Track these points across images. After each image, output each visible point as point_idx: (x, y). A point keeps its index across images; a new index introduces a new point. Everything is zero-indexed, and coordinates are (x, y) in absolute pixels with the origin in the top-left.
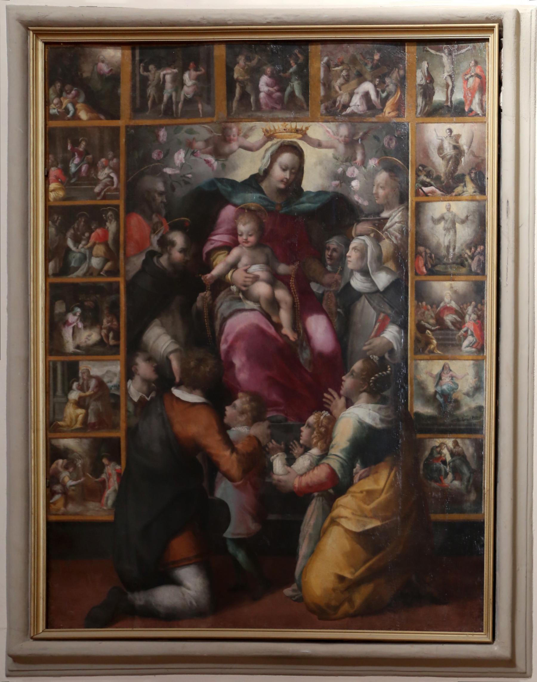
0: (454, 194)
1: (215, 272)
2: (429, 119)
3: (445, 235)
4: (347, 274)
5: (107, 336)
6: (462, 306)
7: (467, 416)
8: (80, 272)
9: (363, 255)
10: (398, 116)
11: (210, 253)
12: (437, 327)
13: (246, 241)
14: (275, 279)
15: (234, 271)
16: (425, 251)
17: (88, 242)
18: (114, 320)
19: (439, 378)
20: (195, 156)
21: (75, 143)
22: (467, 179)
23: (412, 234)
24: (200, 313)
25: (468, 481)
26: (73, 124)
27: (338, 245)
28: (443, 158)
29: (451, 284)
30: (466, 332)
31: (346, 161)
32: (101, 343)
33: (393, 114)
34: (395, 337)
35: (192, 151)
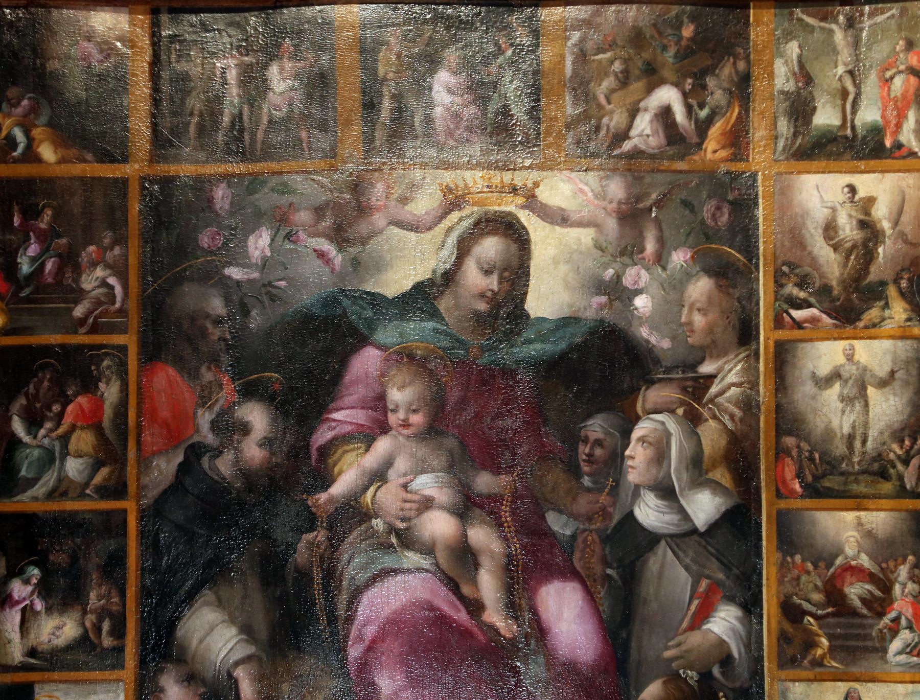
0: (861, 324)
1: (339, 488)
3: (843, 412)
4: (625, 495)
5: (98, 629)
6: (884, 565)
8: (39, 490)
9: (661, 455)
11: (325, 451)
12: (830, 610)
13: (406, 424)
14: (467, 506)
15: (379, 487)
16: (798, 447)
17: (59, 424)
18: (114, 593)
20: (294, 242)
21: (31, 213)
22: (892, 291)
23: (768, 410)
24: (304, 576)
26: (25, 170)
27: (607, 433)
28: (835, 248)
29: (859, 518)
30: (896, 620)
31: (622, 253)
32: (84, 643)
33: (723, 154)
35: (288, 230)
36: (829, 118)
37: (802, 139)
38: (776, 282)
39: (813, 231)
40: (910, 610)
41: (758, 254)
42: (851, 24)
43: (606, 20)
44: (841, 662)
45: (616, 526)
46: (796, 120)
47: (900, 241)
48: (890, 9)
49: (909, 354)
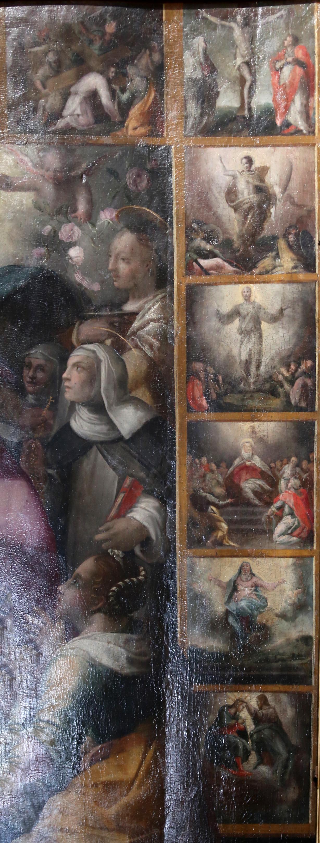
0: (256, 271)
2: (210, 139)
3: (242, 342)
6: (272, 465)
7: (284, 654)
10: (151, 134)
12: (229, 501)
16: (205, 370)
19: (233, 588)
22: (282, 244)
25: (285, 767)
27: (47, 360)
28: (236, 209)
30: (281, 508)
33: (142, 130)
34: (152, 518)
36: (229, 101)
37: (208, 118)
38: (187, 236)
39: (217, 195)
40: (292, 500)
41: (172, 214)
42: (248, 23)
43: (40, 18)
44: (236, 542)
45: (55, 436)
46: (203, 102)
47: (288, 203)
48: (279, 10)
49: (295, 295)
